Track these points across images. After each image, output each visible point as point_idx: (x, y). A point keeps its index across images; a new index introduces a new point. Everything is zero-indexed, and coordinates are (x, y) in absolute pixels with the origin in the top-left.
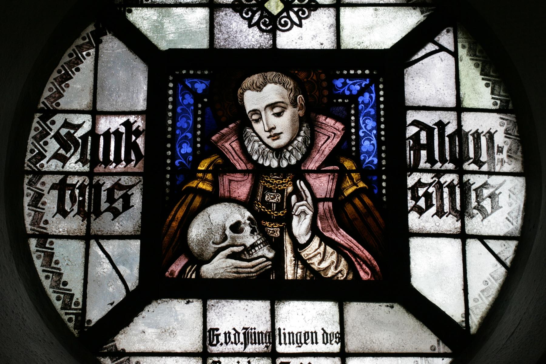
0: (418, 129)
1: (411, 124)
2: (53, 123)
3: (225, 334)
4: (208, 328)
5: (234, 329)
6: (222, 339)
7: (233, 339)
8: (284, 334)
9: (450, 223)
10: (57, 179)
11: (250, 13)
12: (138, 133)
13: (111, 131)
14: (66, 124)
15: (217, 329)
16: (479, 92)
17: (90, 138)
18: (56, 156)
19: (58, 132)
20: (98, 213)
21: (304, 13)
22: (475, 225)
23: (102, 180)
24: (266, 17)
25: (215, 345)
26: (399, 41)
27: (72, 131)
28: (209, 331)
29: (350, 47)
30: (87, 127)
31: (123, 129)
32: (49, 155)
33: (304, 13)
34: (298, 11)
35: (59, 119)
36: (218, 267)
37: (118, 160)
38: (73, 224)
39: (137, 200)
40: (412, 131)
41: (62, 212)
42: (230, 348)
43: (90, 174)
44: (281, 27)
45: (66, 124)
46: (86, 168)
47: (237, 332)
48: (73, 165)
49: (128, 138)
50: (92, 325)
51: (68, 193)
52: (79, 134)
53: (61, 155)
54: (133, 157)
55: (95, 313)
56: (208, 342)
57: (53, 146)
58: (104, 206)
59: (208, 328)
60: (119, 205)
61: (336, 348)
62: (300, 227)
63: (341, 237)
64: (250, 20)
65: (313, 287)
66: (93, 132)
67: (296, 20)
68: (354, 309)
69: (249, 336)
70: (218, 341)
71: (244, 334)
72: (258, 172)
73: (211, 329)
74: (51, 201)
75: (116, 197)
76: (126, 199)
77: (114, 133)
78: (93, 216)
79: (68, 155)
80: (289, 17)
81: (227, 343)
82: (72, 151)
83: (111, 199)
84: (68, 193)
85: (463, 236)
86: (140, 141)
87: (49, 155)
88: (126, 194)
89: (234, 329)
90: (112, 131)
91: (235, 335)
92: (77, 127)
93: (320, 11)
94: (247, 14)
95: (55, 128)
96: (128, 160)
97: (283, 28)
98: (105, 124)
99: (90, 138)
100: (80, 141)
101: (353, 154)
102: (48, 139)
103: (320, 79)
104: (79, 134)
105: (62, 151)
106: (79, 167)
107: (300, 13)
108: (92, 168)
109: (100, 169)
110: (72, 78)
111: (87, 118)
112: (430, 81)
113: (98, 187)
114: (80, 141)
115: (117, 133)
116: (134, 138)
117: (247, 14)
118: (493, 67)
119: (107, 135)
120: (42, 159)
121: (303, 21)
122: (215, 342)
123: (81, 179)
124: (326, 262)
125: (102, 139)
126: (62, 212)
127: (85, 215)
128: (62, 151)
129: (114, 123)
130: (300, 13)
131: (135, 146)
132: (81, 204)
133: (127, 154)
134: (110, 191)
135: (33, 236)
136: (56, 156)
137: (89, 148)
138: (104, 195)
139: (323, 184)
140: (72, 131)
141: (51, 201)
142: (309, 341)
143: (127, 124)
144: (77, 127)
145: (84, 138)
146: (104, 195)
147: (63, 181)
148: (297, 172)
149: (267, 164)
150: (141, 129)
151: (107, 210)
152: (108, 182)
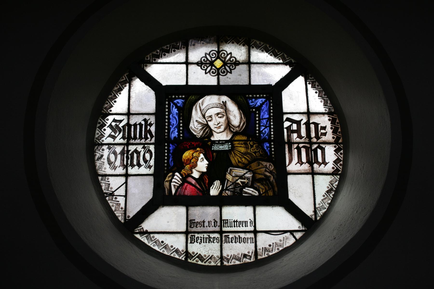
0: (291, 123)
1: (286, 121)
2: (108, 120)
5: (214, 220)
8: (230, 222)
11: (206, 67)
15: (194, 220)
16: (317, 104)
17: (127, 127)
18: (110, 136)
21: (233, 67)
25: (193, 228)
26: (296, 78)
27: (118, 124)
28: (190, 221)
31: (143, 123)
32: (106, 135)
33: (233, 67)
34: (230, 66)
37: (141, 138)
40: (287, 124)
44: (221, 74)
45: (114, 120)
47: (215, 221)
48: (119, 140)
50: (130, 218)
52: (121, 125)
53: (112, 135)
54: (149, 136)
55: (132, 212)
56: (189, 226)
57: (108, 131)
61: (252, 229)
67: (229, 70)
68: (260, 210)
73: (191, 220)
77: (138, 124)
79: (116, 136)
80: (225, 68)
81: (215, 226)
85: (313, 173)
87: (106, 135)
89: (214, 220)
90: (137, 123)
91: (214, 222)
92: (121, 121)
93: (240, 66)
94: (233, 60)
95: (109, 122)
96: (146, 138)
98: (134, 120)
99: (127, 127)
100: (122, 128)
101: (257, 135)
102: (105, 128)
105: (113, 134)
106: (122, 141)
107: (231, 67)
108: (128, 141)
110: (117, 97)
111: (125, 117)
114: (122, 128)
116: (149, 127)
117: (204, 68)
118: (327, 93)
119: (135, 125)
120: (103, 137)
121: (232, 71)
122: (193, 226)
125: (133, 127)
128: (113, 134)
130: (231, 67)
136: (110, 136)
137: (126, 131)
142: (241, 225)
144: (121, 121)
149: (198, 53)
150: (152, 123)
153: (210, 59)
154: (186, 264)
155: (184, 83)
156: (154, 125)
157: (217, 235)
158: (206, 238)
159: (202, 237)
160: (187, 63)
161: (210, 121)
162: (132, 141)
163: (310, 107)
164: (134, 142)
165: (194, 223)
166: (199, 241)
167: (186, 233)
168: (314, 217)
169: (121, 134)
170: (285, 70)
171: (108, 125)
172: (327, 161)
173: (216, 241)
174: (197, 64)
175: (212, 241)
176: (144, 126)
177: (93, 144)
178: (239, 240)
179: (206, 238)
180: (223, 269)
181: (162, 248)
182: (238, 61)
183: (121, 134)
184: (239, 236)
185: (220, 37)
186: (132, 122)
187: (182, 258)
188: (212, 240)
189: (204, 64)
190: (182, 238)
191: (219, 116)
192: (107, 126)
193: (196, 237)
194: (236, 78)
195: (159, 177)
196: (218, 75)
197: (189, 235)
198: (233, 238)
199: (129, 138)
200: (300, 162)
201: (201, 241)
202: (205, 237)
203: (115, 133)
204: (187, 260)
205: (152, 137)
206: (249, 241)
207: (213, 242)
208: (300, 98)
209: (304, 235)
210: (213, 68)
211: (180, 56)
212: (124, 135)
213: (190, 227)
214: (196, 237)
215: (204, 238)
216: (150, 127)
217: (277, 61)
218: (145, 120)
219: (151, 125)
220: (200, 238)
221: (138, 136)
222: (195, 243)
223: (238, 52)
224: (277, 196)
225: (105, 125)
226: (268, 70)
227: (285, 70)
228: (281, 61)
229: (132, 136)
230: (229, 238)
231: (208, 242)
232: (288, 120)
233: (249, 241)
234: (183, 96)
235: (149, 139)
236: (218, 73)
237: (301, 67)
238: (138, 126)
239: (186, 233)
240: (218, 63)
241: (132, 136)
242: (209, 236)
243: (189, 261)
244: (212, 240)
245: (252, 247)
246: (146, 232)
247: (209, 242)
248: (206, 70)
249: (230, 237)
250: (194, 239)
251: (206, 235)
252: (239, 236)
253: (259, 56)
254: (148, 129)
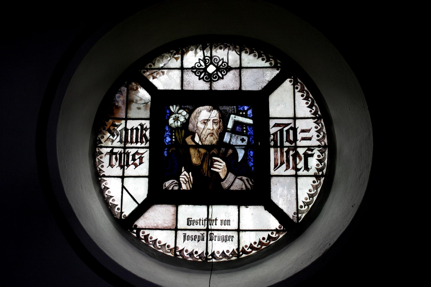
10: (109, 150)
12: (146, 129)
13: (134, 128)
15: (191, 219)
16: (303, 109)
20: (128, 165)
21: (224, 73)
23: (130, 150)
24: (216, 63)
29: (190, 88)
31: (139, 127)
38: (117, 171)
39: (146, 160)
41: (111, 165)
43: (125, 148)
46: (122, 145)
49: (142, 132)
51: (114, 156)
52: (119, 129)
58: (131, 162)
60: (137, 162)
64: (199, 76)
70: (191, 224)
74: (106, 160)
75: (136, 158)
76: (141, 158)
77: (135, 129)
78: (126, 167)
79: (114, 139)
80: (217, 74)
83: (134, 159)
84: (114, 156)
86: (148, 133)
88: (141, 157)
94: (198, 74)
97: (216, 79)
99: (124, 132)
104: (119, 129)
106: (119, 144)
107: (223, 72)
108: (125, 145)
109: (128, 145)
113: (128, 154)
115: (137, 129)
116: (144, 132)
119: (132, 129)
123: (120, 150)
126: (111, 165)
127: (122, 167)
128: (111, 137)
131: (145, 135)
132: (120, 162)
133: (141, 138)
134: (134, 155)
135: (190, 168)
138: (131, 158)
141: (106, 160)
143: (142, 125)
146: (131, 158)
147: (112, 151)
149: (192, 58)
151: (132, 164)
152: (133, 151)
156: (148, 131)
160: (240, 68)
162: (128, 145)
164: (136, 146)
165: (191, 221)
166: (197, 240)
169: (119, 137)
170: (271, 74)
172: (309, 167)
174: (192, 68)
176: (140, 131)
178: (225, 239)
180: (204, 265)
182: (230, 66)
183: (119, 137)
185: (206, 42)
186: (129, 127)
193: (214, 235)
194: (227, 83)
195: (155, 179)
200: (288, 167)
203: (113, 136)
208: (287, 104)
216: (146, 131)
217: (268, 64)
218: (142, 125)
219: (146, 129)
224: (157, 195)
228: (268, 64)
229: (129, 140)
232: (276, 125)
238: (135, 131)
240: (211, 69)
241: (129, 140)
248: (199, 76)
253: (249, 59)
254: (144, 133)
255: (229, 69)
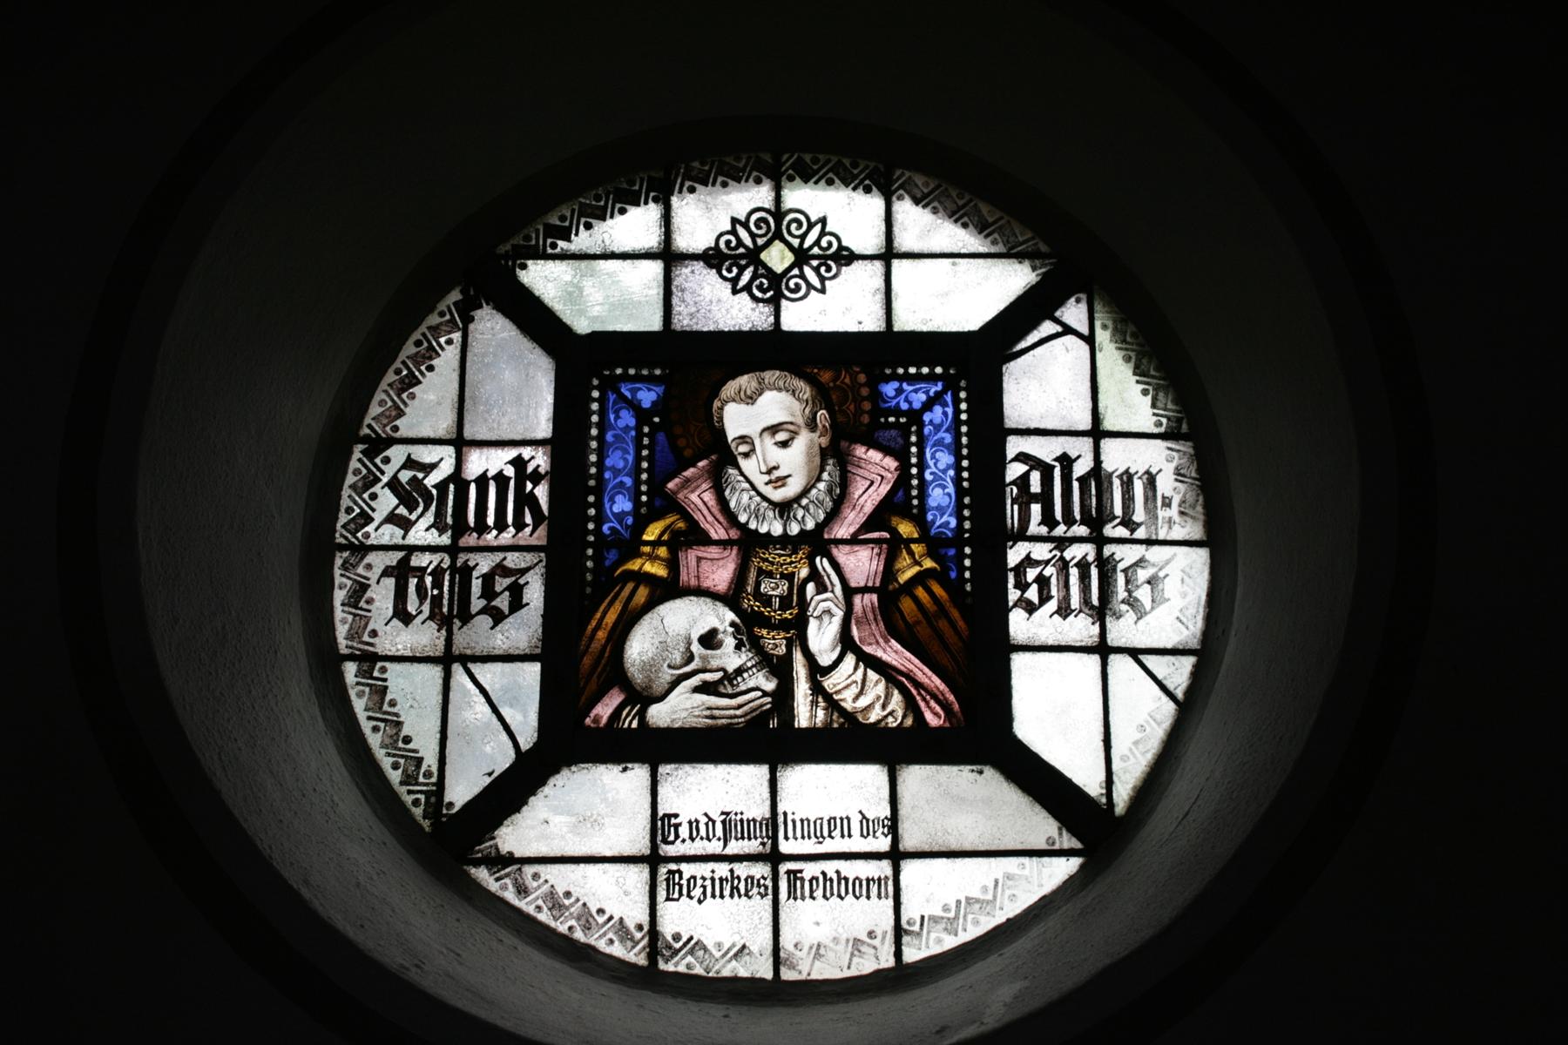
1: (1013, 460)
2: (387, 461)
3: (690, 823)
4: (660, 814)
6: (684, 831)
7: (703, 832)
8: (794, 822)
9: (1081, 628)
11: (735, 270)
12: (536, 478)
14: (410, 463)
15: (676, 816)
16: (1131, 402)
17: (452, 487)
18: (392, 519)
19: (395, 477)
22: (1123, 631)
25: (672, 843)
27: (420, 475)
28: (662, 819)
30: (446, 468)
31: (510, 471)
32: (378, 517)
34: (736, 248)
35: (397, 454)
36: (678, 709)
37: (501, 526)
40: (1015, 471)
42: (699, 847)
43: (453, 550)
45: (410, 463)
46: (445, 540)
48: (422, 533)
53: (401, 517)
54: (528, 519)
57: (387, 501)
59: (660, 814)
62: (822, 637)
63: (894, 654)
65: (846, 741)
66: (457, 477)
68: (915, 777)
69: (731, 826)
70: (677, 836)
71: (724, 822)
72: (749, 543)
73: (665, 815)
77: (494, 478)
79: (413, 517)
82: (420, 509)
85: (1103, 649)
86: (542, 492)
93: (857, 266)
95: (390, 470)
96: (519, 525)
98: (479, 463)
99: (452, 487)
100: (434, 492)
102: (377, 489)
103: (854, 381)
105: (402, 511)
106: (433, 538)
107: (823, 269)
108: (455, 538)
109: (470, 540)
111: (448, 452)
112: (1049, 386)
113: (467, 571)
114: (434, 492)
115: (501, 479)
116: (529, 486)
118: (1158, 360)
119: (482, 481)
120: (366, 524)
122: (672, 838)
124: (867, 697)
125: (473, 487)
128: (402, 511)
129: (494, 461)
130: (823, 269)
136: (392, 519)
139: (861, 564)
140: (420, 475)
142: (837, 833)
143: (518, 463)
145: (442, 486)
148: (816, 543)
149: (703, 217)
150: (542, 471)
153: (748, 241)
154: (654, 976)
155: (654, 323)
157: (760, 870)
158: (721, 879)
159: (708, 875)
160: (888, 254)
161: (746, 455)
163: (627, 852)
166: (697, 892)
167: (653, 860)
168: (1104, 800)
170: (1011, 280)
171: (385, 479)
173: (755, 890)
175: (743, 891)
176: (512, 483)
177: (321, 547)
179: (721, 879)
181: (572, 905)
184: (838, 872)
187: (635, 956)
188: (742, 887)
189: (727, 257)
190: (637, 876)
191: (782, 436)
192: (380, 485)
193: (686, 876)
194: (839, 307)
196: (778, 213)
197: (663, 870)
198: (817, 879)
199: (460, 528)
201: (704, 893)
202: (717, 876)
204: (656, 963)
205: (538, 518)
206: (874, 889)
207: (746, 895)
209: (1082, 867)
210: (796, 242)
211: (635, 226)
212: (440, 514)
213: (665, 842)
214: (686, 876)
215: (713, 879)
220: (699, 882)
221: (490, 521)
222: (684, 899)
223: (850, 213)
225: (378, 480)
226: (954, 282)
227: (1011, 280)
230: (802, 879)
231: (727, 892)
233: (874, 889)
234: (658, 372)
235: (528, 530)
236: (774, 289)
237: (1074, 263)
239: (653, 860)
242: (732, 871)
243: (662, 966)
244: (742, 887)
245: (878, 913)
246: (510, 859)
247: (732, 896)
248: (823, 233)
249: (807, 875)
250: (681, 886)
251: (722, 870)
252: (838, 872)
253: (918, 224)
255: (845, 257)
